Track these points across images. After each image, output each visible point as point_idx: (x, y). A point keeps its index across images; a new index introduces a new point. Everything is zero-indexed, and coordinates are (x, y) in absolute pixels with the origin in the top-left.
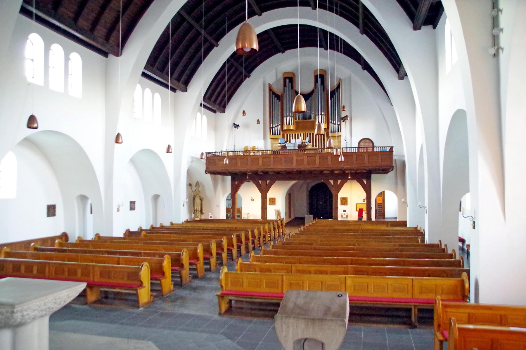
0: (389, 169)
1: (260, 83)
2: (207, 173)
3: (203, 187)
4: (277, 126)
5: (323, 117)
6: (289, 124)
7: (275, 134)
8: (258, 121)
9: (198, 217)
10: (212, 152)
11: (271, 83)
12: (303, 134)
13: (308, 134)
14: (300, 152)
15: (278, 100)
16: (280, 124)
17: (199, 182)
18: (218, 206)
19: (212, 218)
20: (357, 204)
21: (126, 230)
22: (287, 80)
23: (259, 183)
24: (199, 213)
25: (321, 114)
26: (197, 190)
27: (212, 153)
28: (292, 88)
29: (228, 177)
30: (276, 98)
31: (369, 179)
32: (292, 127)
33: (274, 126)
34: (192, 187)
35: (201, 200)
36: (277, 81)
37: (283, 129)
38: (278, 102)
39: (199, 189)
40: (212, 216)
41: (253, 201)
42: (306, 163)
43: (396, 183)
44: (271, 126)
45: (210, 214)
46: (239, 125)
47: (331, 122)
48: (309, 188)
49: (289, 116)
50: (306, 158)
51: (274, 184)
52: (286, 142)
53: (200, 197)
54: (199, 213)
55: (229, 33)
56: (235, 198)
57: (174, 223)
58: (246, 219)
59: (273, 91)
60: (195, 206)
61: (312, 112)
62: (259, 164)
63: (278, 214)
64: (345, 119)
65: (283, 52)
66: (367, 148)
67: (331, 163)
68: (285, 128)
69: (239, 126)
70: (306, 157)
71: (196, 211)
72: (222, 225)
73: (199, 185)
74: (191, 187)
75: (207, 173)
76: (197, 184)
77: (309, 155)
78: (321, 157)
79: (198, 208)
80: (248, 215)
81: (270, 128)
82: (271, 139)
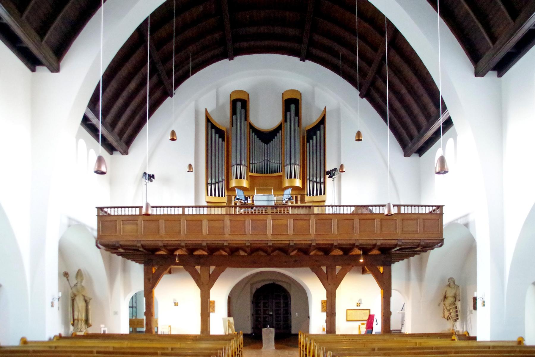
1: (191, 107)
3: (90, 281)
7: (215, 195)
8: (190, 166)
9: (81, 331)
11: (209, 111)
16: (223, 178)
18: (116, 313)
21: (473, 299)
22: (239, 105)
23: (196, 270)
26: (79, 285)
27: (105, 210)
30: (217, 136)
32: (245, 183)
34: (69, 278)
35: (87, 302)
36: (220, 108)
39: (81, 282)
41: (177, 305)
42: (291, 231)
43: (408, 279)
44: (209, 181)
45: (102, 326)
46: (153, 176)
48: (254, 291)
50: (291, 222)
51: (223, 272)
53: (84, 296)
56: (152, 297)
60: (76, 313)
63: (229, 325)
64: (331, 174)
67: (337, 233)
69: (154, 178)
70: (292, 221)
71: (78, 320)
72: (126, 344)
73: (82, 276)
74: (67, 278)
76: (79, 274)
77: (296, 218)
79: (81, 316)
80: (170, 327)
81: (207, 184)
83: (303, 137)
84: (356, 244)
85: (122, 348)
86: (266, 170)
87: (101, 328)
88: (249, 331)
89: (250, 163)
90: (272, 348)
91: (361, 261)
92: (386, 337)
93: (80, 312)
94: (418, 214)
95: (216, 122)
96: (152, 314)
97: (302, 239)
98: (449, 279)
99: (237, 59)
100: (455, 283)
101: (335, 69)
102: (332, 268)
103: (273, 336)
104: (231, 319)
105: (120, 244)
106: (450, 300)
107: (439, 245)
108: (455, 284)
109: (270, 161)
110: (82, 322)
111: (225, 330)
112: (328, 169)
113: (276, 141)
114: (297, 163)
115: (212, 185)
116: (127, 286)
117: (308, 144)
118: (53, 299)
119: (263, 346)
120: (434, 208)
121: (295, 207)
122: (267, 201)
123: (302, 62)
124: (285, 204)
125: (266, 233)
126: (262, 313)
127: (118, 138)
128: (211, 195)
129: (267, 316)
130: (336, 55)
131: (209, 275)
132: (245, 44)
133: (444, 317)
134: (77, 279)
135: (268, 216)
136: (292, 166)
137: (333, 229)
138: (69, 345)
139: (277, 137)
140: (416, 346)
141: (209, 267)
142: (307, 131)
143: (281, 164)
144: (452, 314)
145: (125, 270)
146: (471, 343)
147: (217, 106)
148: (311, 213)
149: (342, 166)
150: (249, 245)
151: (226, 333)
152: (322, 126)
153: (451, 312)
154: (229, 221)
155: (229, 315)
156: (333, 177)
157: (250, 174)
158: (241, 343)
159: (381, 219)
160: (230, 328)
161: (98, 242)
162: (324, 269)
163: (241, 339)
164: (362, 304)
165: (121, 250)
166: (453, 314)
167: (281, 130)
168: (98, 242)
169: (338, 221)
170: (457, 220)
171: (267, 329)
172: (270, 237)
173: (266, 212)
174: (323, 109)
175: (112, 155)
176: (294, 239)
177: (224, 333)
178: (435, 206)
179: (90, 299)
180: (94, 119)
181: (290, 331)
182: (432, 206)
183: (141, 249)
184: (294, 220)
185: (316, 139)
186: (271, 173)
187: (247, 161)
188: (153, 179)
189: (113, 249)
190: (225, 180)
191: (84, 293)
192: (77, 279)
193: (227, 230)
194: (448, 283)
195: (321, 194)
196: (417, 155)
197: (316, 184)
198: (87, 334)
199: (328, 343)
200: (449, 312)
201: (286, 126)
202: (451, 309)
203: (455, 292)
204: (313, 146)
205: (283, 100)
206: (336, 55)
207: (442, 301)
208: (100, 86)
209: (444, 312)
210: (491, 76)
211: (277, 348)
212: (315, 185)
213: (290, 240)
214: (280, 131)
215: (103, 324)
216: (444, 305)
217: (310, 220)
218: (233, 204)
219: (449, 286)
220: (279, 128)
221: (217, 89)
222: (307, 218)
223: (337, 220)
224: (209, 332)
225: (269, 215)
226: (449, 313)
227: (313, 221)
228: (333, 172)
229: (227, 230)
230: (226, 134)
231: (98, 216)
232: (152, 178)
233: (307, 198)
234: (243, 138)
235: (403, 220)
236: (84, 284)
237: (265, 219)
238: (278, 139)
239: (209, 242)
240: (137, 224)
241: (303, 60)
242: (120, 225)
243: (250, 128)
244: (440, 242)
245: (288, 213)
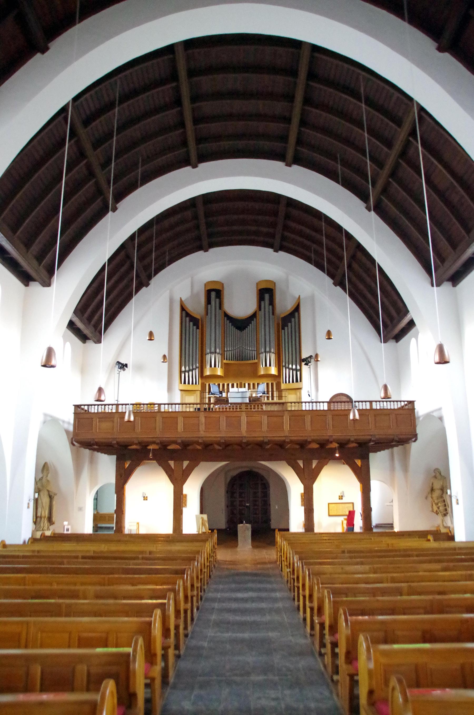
0: (410, 439)
2: (74, 443)
3: (56, 473)
5: (273, 356)
6: (215, 366)
7: (189, 383)
8: (164, 356)
10: (84, 405)
11: (183, 299)
14: (254, 408)
16: (197, 365)
17: (48, 463)
18: (80, 509)
19: (69, 532)
20: (329, 504)
22: (213, 294)
24: (45, 523)
25: (270, 352)
26: (44, 480)
27: (83, 407)
29: (288, 405)
30: (191, 323)
31: (365, 458)
32: (219, 372)
33: (235, 349)
35: (51, 498)
36: (194, 296)
37: (205, 375)
38: (195, 329)
39: (47, 476)
40: (69, 527)
41: (147, 500)
42: (265, 428)
43: (393, 469)
44: (183, 369)
45: (66, 523)
46: (126, 365)
47: (285, 366)
48: (228, 480)
49: (215, 352)
50: (265, 419)
52: (222, 391)
53: (48, 491)
54: (46, 521)
55: (144, 187)
57: (8, 542)
58: (134, 532)
59: (186, 310)
60: (39, 510)
61: (251, 349)
62: (177, 429)
64: (307, 361)
66: (371, 402)
68: (208, 372)
73: (48, 470)
75: (74, 443)
77: (270, 414)
78: (292, 417)
79: (45, 512)
80: (138, 525)
81: (181, 372)
82: (181, 390)
83: (278, 324)
84: (330, 440)
85: (102, 552)
86: (241, 357)
87: (64, 527)
88: (223, 525)
89: (224, 351)
90: (248, 547)
91: (337, 455)
92: (366, 536)
93: (43, 508)
94: (391, 409)
95: (191, 311)
96: (123, 511)
97: (277, 436)
98: (435, 470)
99: (212, 251)
100: (441, 474)
101: (308, 259)
102: (308, 463)
103: (249, 533)
104: (205, 516)
105: (96, 442)
106: (437, 493)
107: (413, 440)
108: (441, 476)
109: (245, 348)
110: (44, 519)
111: (198, 528)
112: (304, 357)
113: (251, 327)
114: (272, 350)
115: (186, 373)
116: (93, 479)
117: (283, 331)
118: (29, 500)
119: (239, 545)
120: (406, 403)
121: (269, 404)
123: (275, 253)
124: (260, 398)
125: (241, 430)
126: (238, 497)
127: (93, 329)
128: (185, 383)
129: (243, 507)
130: (308, 248)
131: (183, 470)
132: (220, 239)
133: (433, 512)
134: (42, 473)
135: (242, 412)
136: (267, 354)
137: (307, 425)
138: (46, 549)
139: (252, 325)
140: (388, 548)
141: (183, 462)
142: (282, 318)
144: (441, 508)
145: (92, 461)
146: (447, 544)
147: (191, 293)
148: (284, 409)
149: (317, 355)
150: (224, 441)
151: (199, 532)
152: (296, 314)
153: (440, 506)
154: (204, 418)
155: (202, 512)
156: (309, 364)
157: (225, 361)
158: (216, 543)
160: (203, 526)
161: (74, 439)
162: (301, 463)
163: (215, 539)
164: (344, 496)
165: (96, 447)
166: (442, 508)
167: (256, 317)
168: (74, 439)
169: (311, 418)
170: (433, 412)
171: (242, 525)
172: (244, 434)
173: (241, 408)
174: (297, 296)
176: (268, 436)
177: (197, 531)
178: (407, 401)
179: (55, 494)
180: (74, 318)
181: (269, 525)
182: (404, 401)
183: (116, 446)
184: (267, 416)
185: (291, 326)
186: (246, 360)
187: (222, 349)
188: (126, 368)
189: (88, 446)
190: (199, 367)
191: (48, 488)
192: (42, 473)
193: (202, 428)
194: (434, 474)
195: (297, 381)
196: (394, 341)
197: (291, 371)
198: (54, 534)
200: (437, 506)
201: (261, 315)
202: (439, 502)
203: (442, 484)
204: (288, 333)
205: (257, 289)
206: (308, 248)
207: (429, 494)
209: (432, 505)
210: (447, 286)
211: (254, 547)
213: (264, 437)
214: (255, 319)
215: (66, 521)
216: (432, 498)
217: (283, 416)
218: (207, 402)
219: (435, 477)
220: (254, 316)
221: (192, 278)
223: (310, 416)
224: (182, 531)
225: (243, 411)
226: (437, 507)
227: (286, 418)
228: (309, 359)
229: (202, 428)
230: (200, 322)
231: (75, 413)
234: (217, 327)
235: (375, 416)
236: (49, 478)
237: (240, 415)
238: (253, 327)
239: (184, 439)
240: (113, 422)
241: (276, 251)
242: (96, 421)
243: (225, 316)
244: (415, 436)
245: (262, 409)
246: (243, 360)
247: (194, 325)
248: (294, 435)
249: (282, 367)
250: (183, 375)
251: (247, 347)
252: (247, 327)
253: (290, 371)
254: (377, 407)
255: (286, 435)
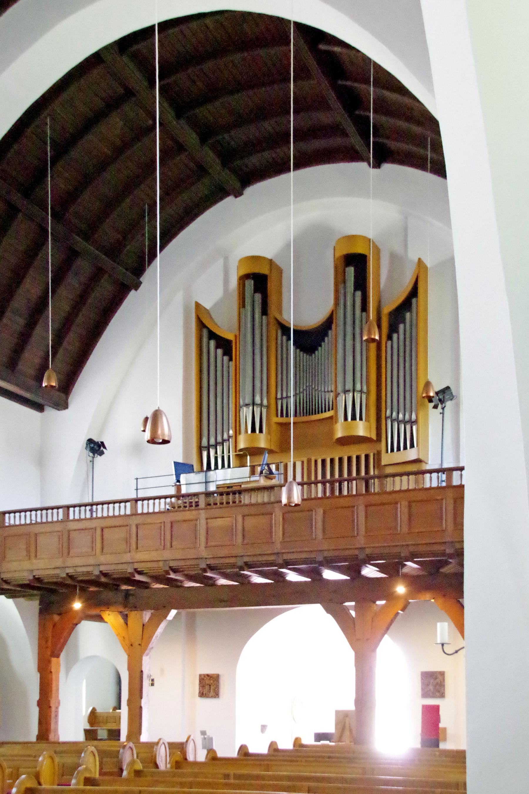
4: (224, 441)
12: (303, 462)
13: (316, 461)
15: (226, 358)
22: (250, 284)
28: (265, 312)
30: (220, 351)
33: (212, 441)
44: (205, 443)
49: (254, 404)
65: (238, 194)
115: (211, 450)
117: (389, 343)
122: (210, 482)
143: (278, 397)
159: (410, 502)
175: (43, 413)
185: (398, 338)
188: (104, 450)
199: (63, 755)
208: (148, 262)
212: (402, 427)
222: (269, 508)
232: (102, 448)
233: (386, 459)
246: (312, 413)
247: (224, 354)
248: (287, 551)
249: (386, 421)
250: (205, 454)
251: (319, 386)
252: (317, 349)
253: (400, 426)
254: (15, 522)
255: (276, 551)
